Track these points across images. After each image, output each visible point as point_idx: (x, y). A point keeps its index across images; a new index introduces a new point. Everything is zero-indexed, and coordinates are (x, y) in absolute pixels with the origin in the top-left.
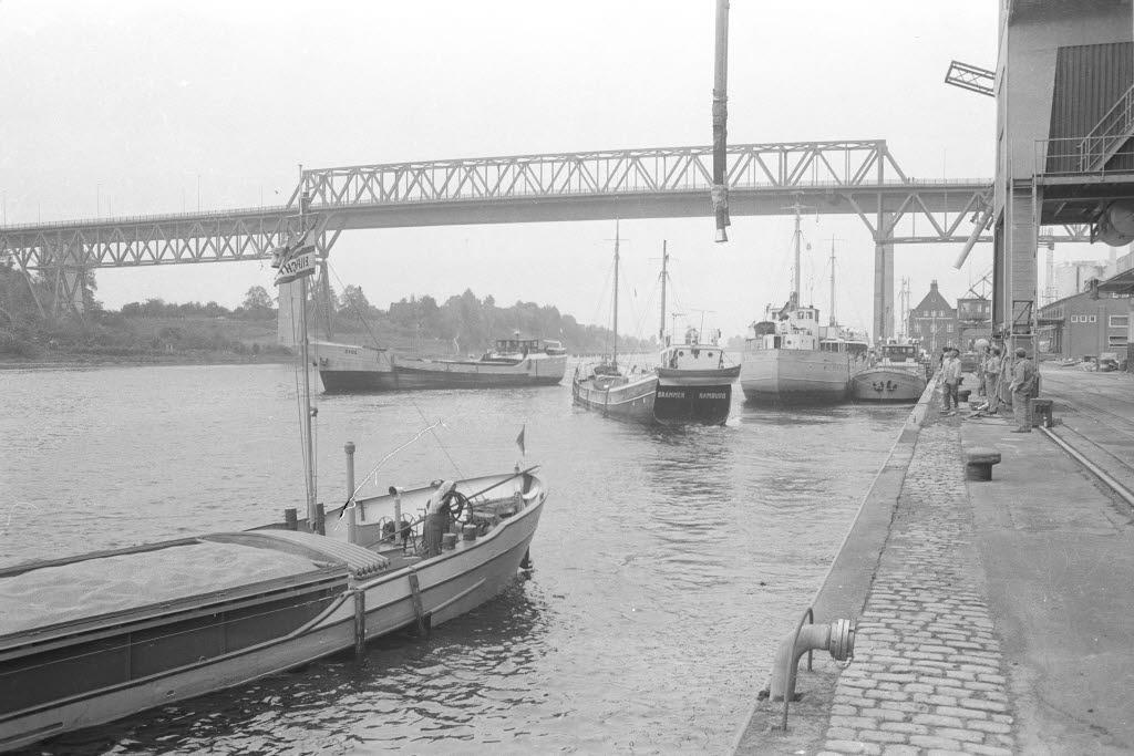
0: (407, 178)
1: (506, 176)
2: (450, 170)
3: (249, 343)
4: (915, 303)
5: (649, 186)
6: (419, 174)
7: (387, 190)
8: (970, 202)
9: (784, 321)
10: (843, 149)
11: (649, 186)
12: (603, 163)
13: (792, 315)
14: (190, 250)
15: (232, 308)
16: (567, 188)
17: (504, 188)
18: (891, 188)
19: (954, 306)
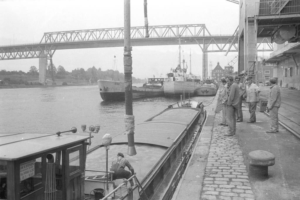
0: (74, 35)
2: (86, 33)
3: (29, 82)
4: (214, 67)
6: (77, 34)
9: (176, 73)
10: (194, 26)
13: (178, 71)
14: (24, 55)
15: (26, 72)
16: (134, 36)
17: (101, 38)
18: (207, 37)
19: (224, 68)
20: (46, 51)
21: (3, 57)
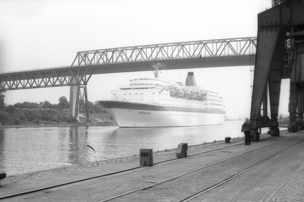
0: (116, 54)
1: (181, 51)
2: (133, 50)
5: (210, 55)
6: (161, 49)
7: (109, 58)
8: (67, 74)
11: (210, 55)
12: (192, 46)
16: (223, 53)
20: (79, 76)
21: (39, 84)
